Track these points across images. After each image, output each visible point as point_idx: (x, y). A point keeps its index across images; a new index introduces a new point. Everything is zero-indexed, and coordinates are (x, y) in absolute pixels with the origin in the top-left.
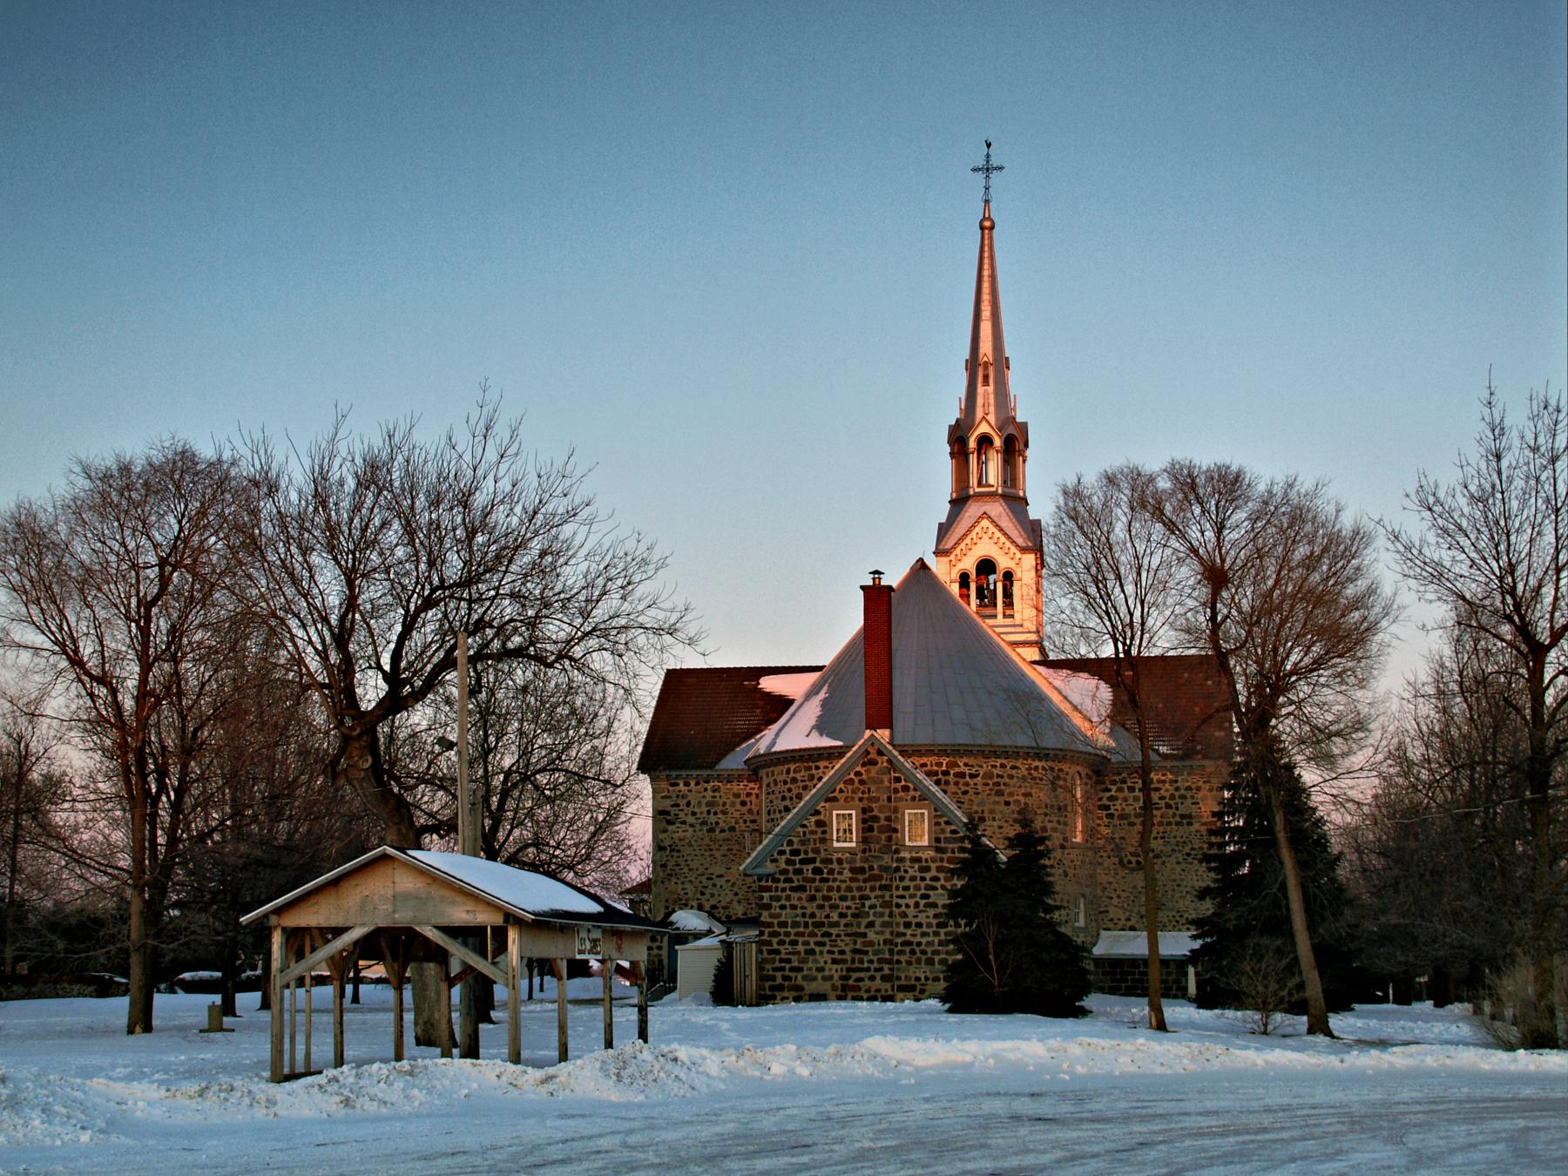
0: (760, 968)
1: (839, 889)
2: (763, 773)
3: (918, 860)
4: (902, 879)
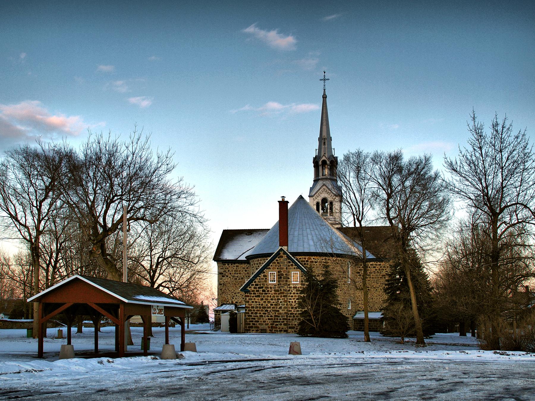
0: (245, 321)
1: (270, 296)
2: (251, 261)
3: (296, 287)
4: (291, 293)
